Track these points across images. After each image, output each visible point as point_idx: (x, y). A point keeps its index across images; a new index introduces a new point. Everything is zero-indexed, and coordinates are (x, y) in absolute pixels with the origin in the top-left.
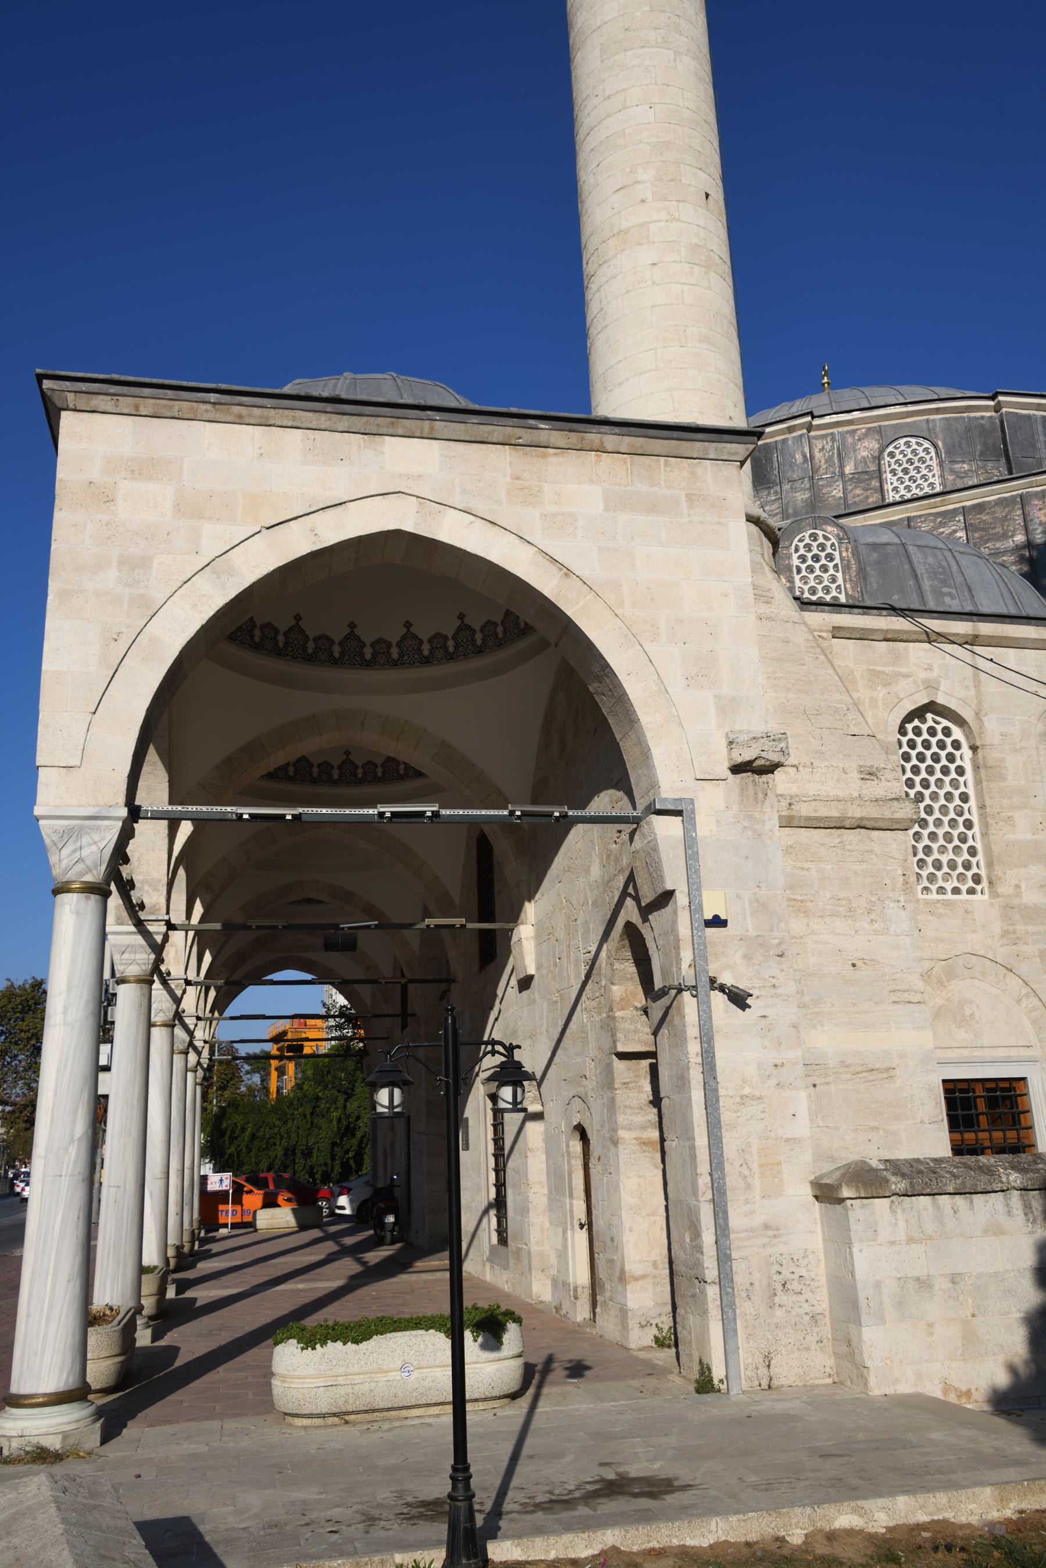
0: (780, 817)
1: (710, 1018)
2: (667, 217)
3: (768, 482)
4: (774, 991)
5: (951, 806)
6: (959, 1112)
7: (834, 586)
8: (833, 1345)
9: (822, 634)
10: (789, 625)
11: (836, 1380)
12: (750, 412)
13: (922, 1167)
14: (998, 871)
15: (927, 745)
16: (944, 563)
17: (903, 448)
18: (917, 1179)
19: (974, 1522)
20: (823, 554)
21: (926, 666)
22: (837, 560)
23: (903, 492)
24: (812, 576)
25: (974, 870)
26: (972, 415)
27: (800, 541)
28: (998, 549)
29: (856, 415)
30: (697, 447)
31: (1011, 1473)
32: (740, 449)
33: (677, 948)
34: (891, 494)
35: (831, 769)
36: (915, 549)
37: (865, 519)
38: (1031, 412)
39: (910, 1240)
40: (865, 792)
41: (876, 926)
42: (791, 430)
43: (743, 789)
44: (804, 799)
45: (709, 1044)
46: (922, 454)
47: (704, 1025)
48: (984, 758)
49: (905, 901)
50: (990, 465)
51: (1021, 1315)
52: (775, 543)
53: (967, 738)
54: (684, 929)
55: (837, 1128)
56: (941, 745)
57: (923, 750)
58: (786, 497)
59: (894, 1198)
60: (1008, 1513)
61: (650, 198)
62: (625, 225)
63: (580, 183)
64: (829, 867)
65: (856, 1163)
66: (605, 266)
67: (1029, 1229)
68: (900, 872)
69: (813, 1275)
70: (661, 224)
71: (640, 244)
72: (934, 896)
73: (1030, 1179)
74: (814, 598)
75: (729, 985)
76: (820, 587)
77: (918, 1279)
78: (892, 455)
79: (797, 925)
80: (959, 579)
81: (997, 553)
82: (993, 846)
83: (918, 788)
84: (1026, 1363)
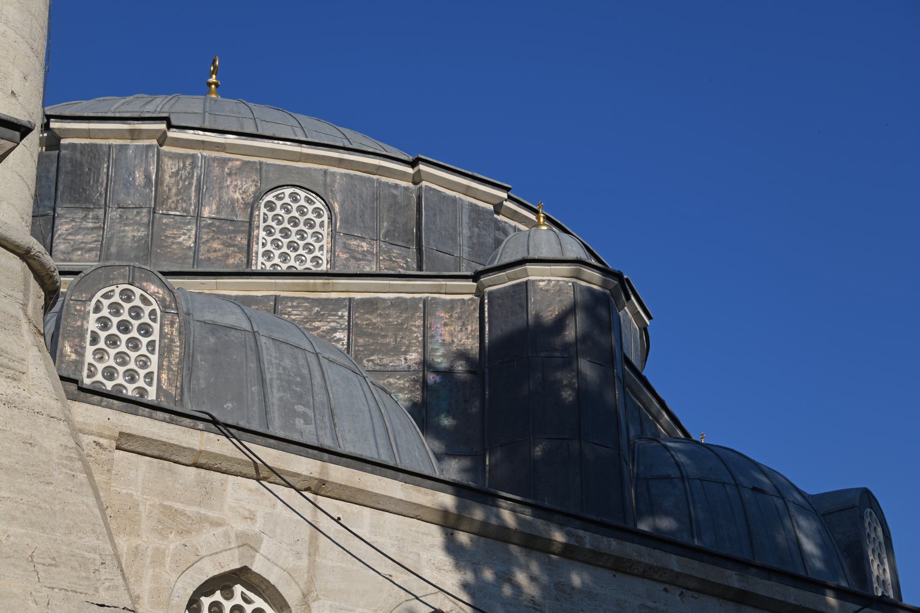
3: (88, 200)
7: (142, 372)
9: (101, 441)
10: (42, 420)
12: (50, 94)
16: (305, 371)
17: (287, 200)
20: (136, 323)
21: (247, 514)
22: (155, 336)
23: (277, 260)
26: (384, 179)
28: (385, 365)
29: (231, 139)
34: (261, 259)
37: (217, 286)
38: (458, 195)
42: (134, 135)
50: (396, 251)
52: (51, 294)
58: (111, 227)
74: (109, 385)
78: (270, 206)
80: (320, 397)
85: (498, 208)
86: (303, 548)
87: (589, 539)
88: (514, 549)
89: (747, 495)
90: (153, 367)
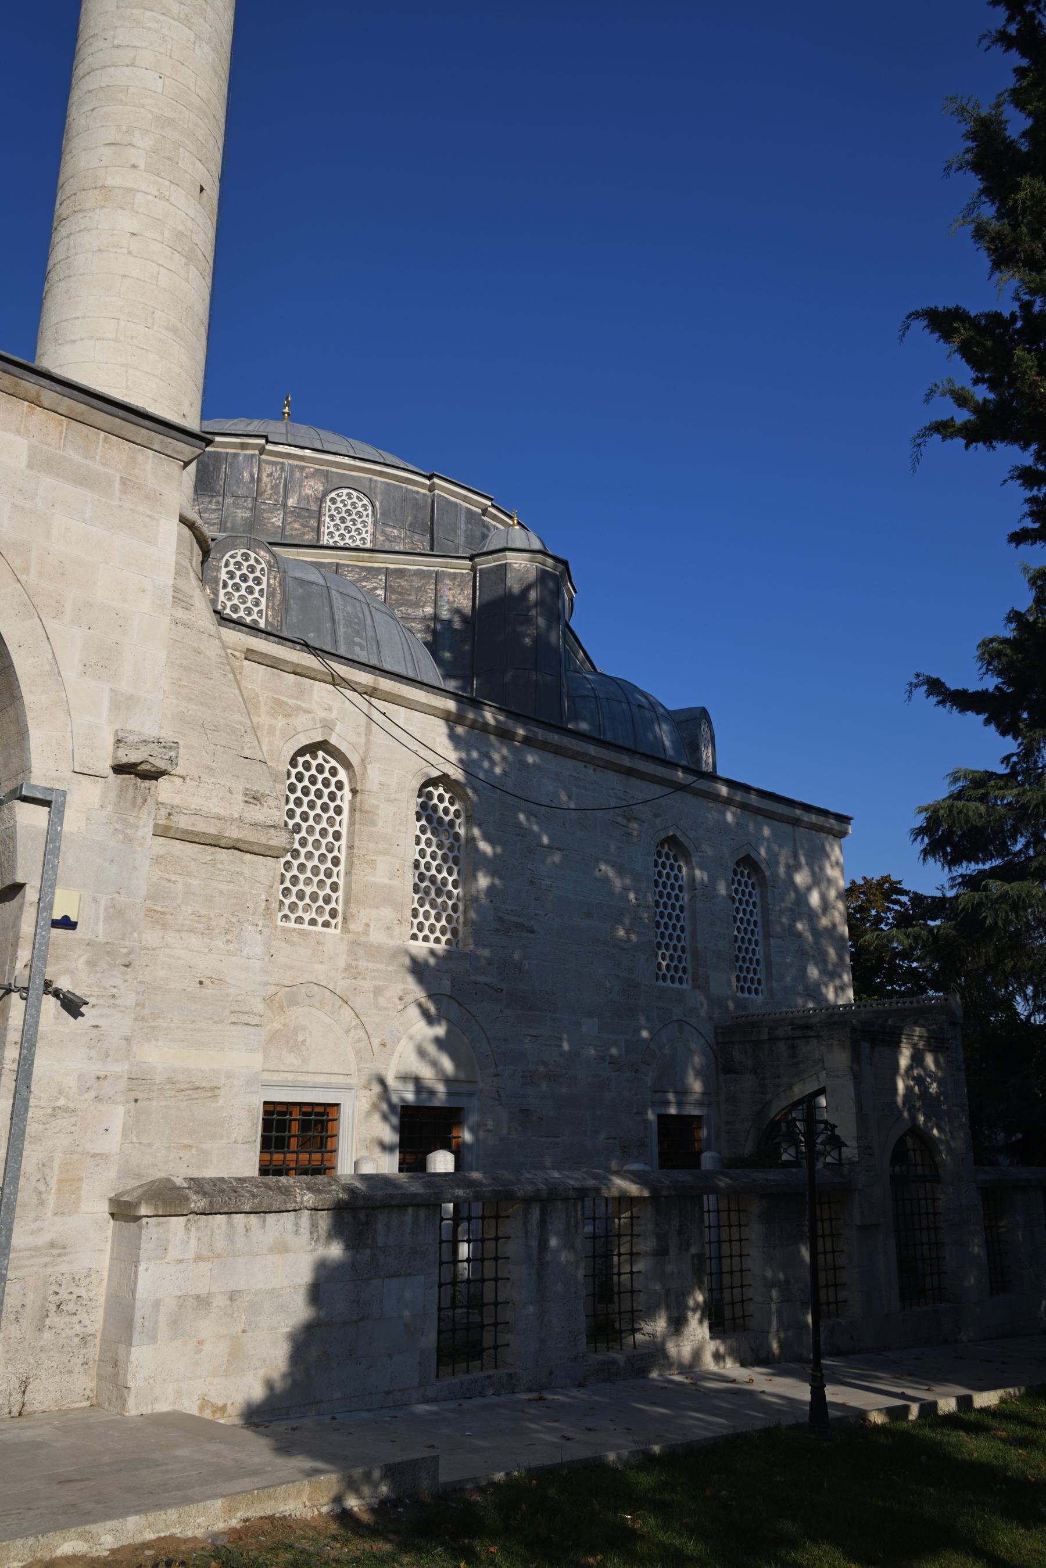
0: (156, 826)
1: (37, 1023)
2: (156, 193)
3: (212, 490)
4: (112, 1001)
5: (324, 842)
6: (274, 1133)
7: (256, 609)
8: (99, 1366)
9: (236, 653)
11: (95, 1402)
12: (205, 415)
13: (224, 1186)
14: (353, 908)
15: (313, 780)
16: (361, 615)
17: (344, 497)
18: (218, 1198)
19: (198, 1536)
20: (251, 576)
22: (264, 586)
23: (337, 539)
24: (237, 595)
25: (333, 905)
26: (410, 487)
27: (232, 557)
30: (142, 434)
31: (246, 1483)
32: (187, 450)
33: (15, 945)
34: (326, 537)
35: (218, 786)
36: (338, 595)
37: (298, 554)
39: (199, 1258)
40: (246, 815)
41: (231, 946)
42: (244, 446)
43: (122, 790)
44: (185, 811)
45: (29, 1050)
46: (360, 509)
47: (29, 1030)
48: (361, 802)
49: (263, 926)
50: (416, 537)
51: (288, 1329)
52: (206, 553)
53: (350, 781)
54: (27, 926)
55: (150, 1145)
56: (326, 783)
57: (308, 784)
58: (227, 509)
59: (191, 1216)
60: (234, 1523)
61: (142, 166)
62: (109, 182)
63: (70, 119)
64: (197, 882)
65: (161, 1180)
66: (80, 215)
67: (311, 1247)
68: (264, 897)
69: (92, 1295)
70: (149, 197)
71: (122, 208)
72: (292, 925)
73: (321, 1200)
74: (235, 616)
75: (65, 990)
76: (242, 607)
77: (198, 1297)
79: (151, 937)
80: (371, 633)
81: (407, 618)
82: (353, 885)
83: (297, 819)
84: (284, 1376)
85: (485, 512)
86: (362, 730)
87: (541, 734)
88: (492, 737)
89: (634, 709)
90: (263, 606)
